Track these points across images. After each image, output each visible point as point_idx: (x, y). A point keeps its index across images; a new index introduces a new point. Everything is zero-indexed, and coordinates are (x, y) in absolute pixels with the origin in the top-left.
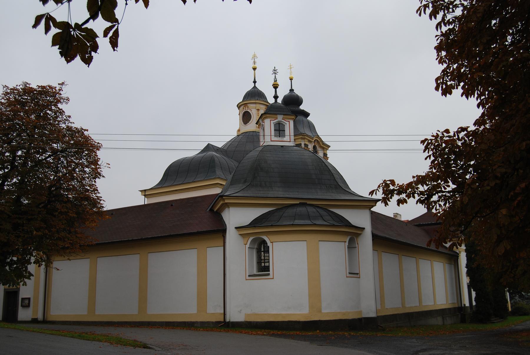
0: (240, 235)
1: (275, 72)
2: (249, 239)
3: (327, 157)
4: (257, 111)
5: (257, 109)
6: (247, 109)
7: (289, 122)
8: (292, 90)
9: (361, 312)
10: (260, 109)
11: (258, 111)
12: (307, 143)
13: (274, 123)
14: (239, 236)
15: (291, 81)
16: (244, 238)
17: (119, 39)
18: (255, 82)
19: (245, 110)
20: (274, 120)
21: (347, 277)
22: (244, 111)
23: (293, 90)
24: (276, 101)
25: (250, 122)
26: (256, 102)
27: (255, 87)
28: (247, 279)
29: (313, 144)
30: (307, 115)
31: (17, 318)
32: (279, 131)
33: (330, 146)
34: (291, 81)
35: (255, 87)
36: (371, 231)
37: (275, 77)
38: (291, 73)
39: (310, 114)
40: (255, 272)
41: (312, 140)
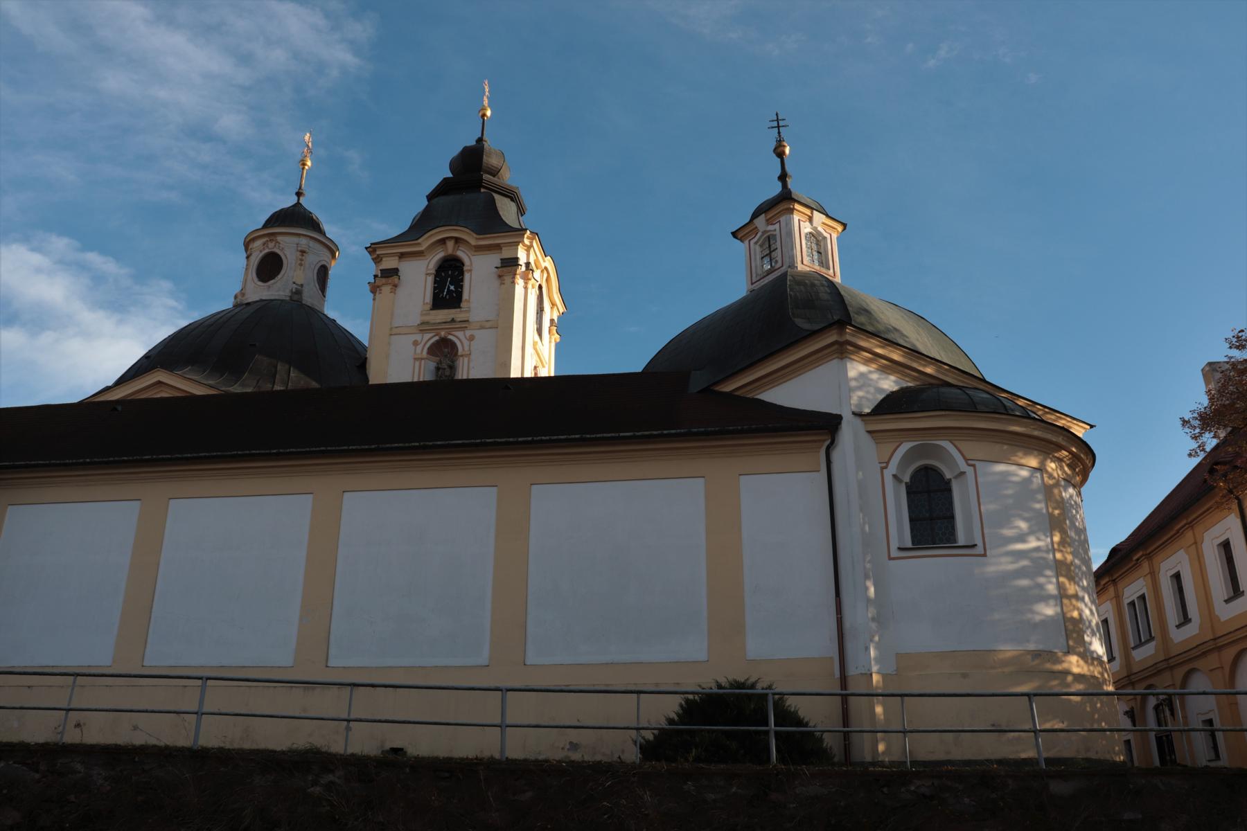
0: (869, 432)
1: (778, 124)
2: (899, 449)
8: (480, 140)
14: (867, 437)
16: (877, 443)
17: (76, 401)
28: (892, 556)
31: (531, 378)
36: (872, 312)
37: (779, 133)
40: (909, 545)
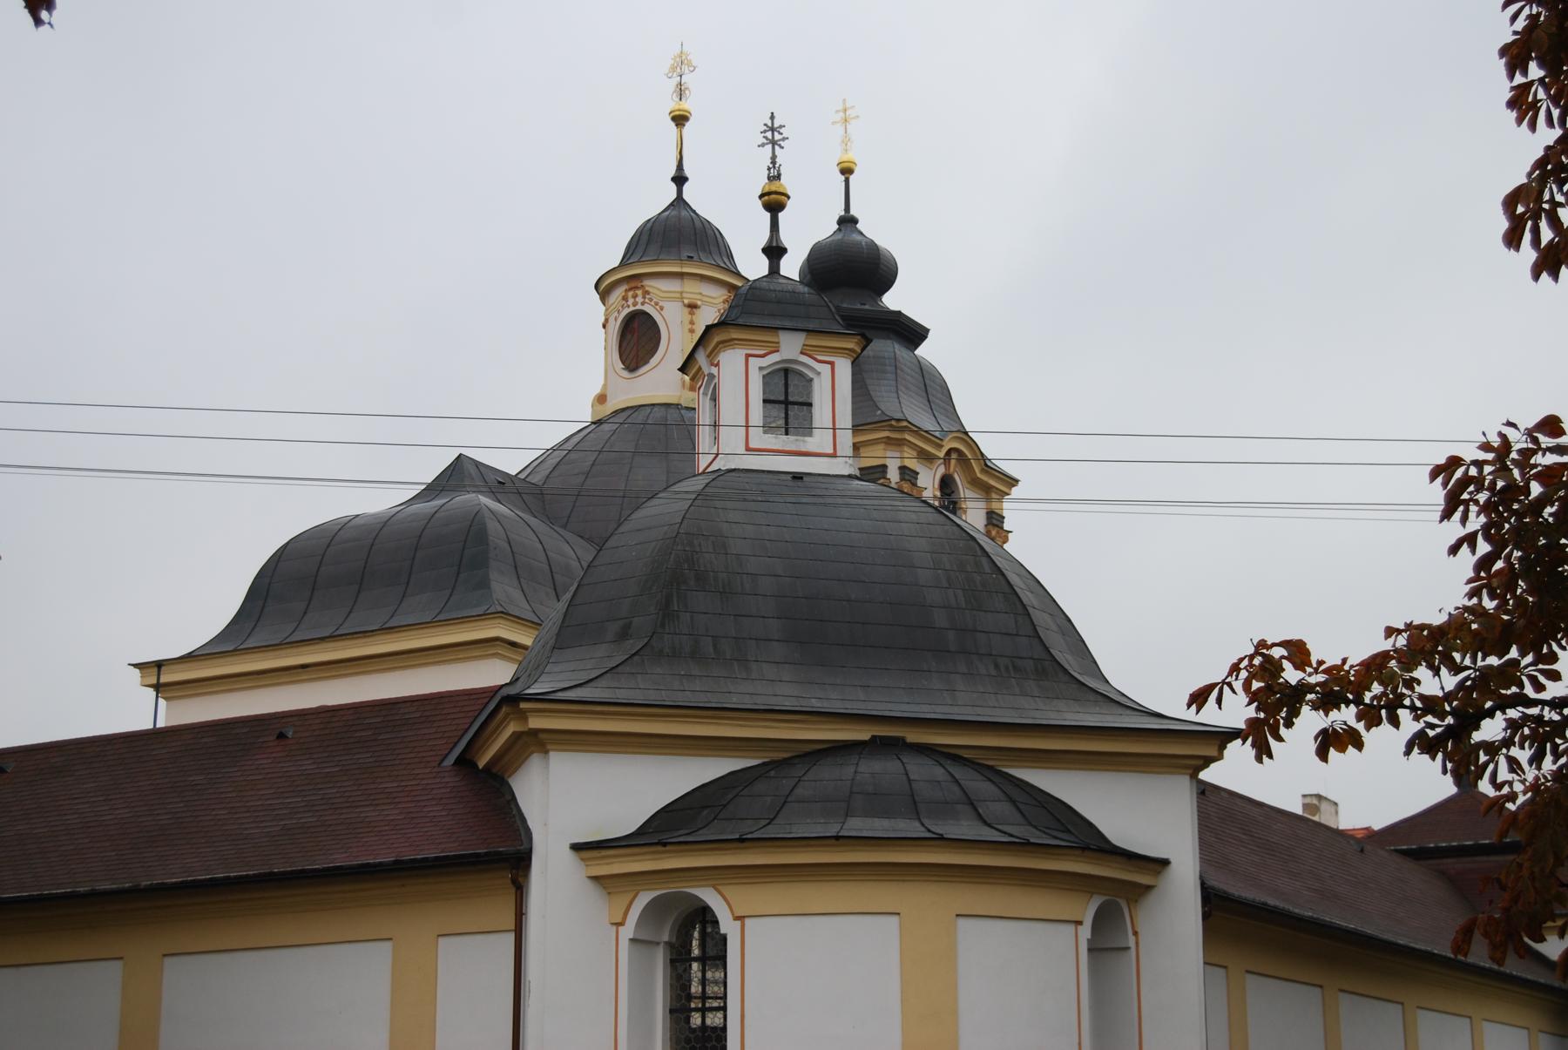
1: (773, 135)
4: (687, 310)
5: (686, 301)
6: (639, 299)
7: (832, 364)
8: (847, 221)
10: (699, 303)
11: (692, 314)
12: (912, 464)
15: (847, 181)
18: (680, 179)
23: (854, 221)
24: (774, 270)
25: (654, 361)
26: (686, 270)
27: (679, 200)
30: (913, 334)
33: (1017, 481)
34: (847, 181)
35: (679, 200)
38: (846, 141)
39: (927, 331)
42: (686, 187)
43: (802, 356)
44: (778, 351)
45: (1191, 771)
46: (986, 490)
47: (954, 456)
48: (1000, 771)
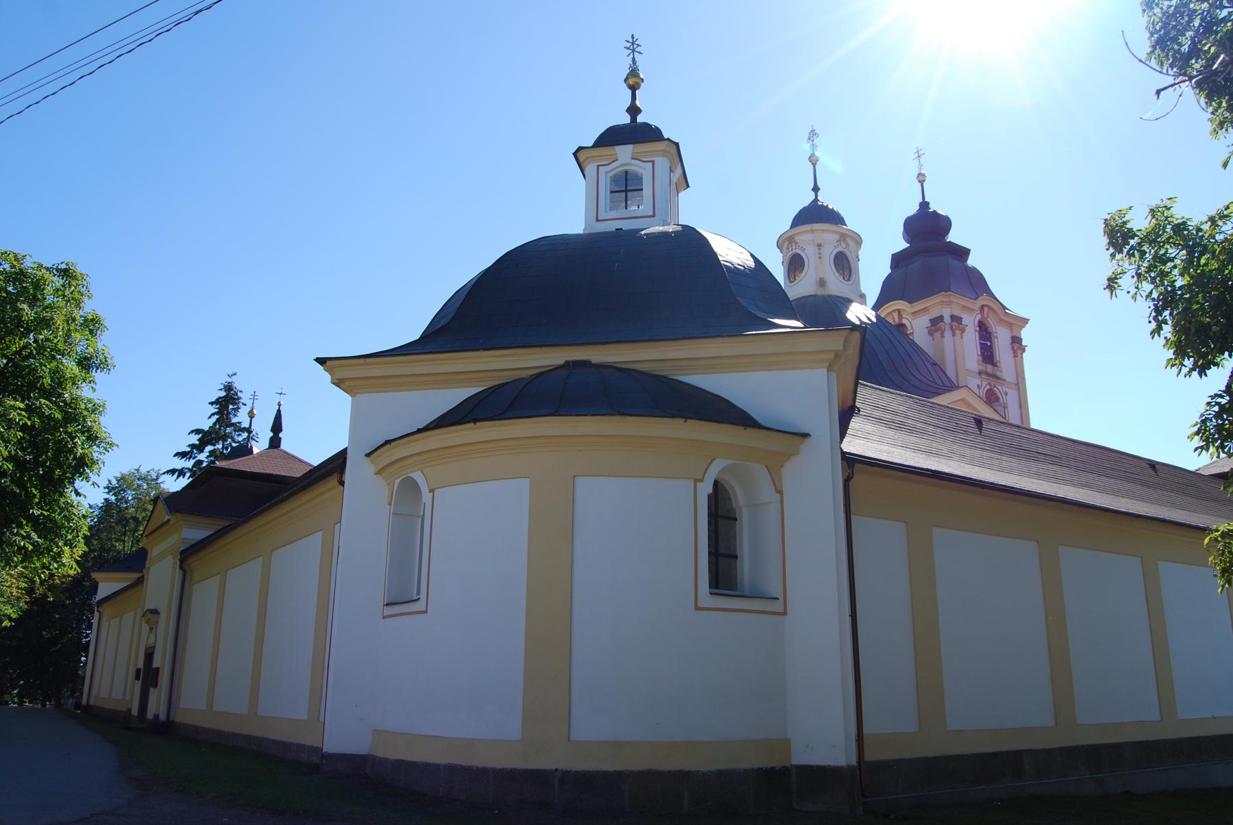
3: (1021, 344)
4: (817, 248)
6: (794, 247)
7: (653, 162)
8: (924, 205)
9: (785, 744)
12: (957, 312)
13: (607, 172)
18: (816, 189)
19: (792, 250)
20: (608, 164)
21: (697, 608)
22: (789, 254)
24: (634, 119)
27: (816, 200)
29: (979, 317)
30: (963, 253)
32: (628, 193)
33: (1028, 320)
38: (920, 166)
39: (969, 250)
41: (973, 307)
42: (628, 103)
43: (633, 160)
44: (617, 160)
45: (827, 364)
46: (1010, 326)
47: (986, 309)
48: (672, 379)
